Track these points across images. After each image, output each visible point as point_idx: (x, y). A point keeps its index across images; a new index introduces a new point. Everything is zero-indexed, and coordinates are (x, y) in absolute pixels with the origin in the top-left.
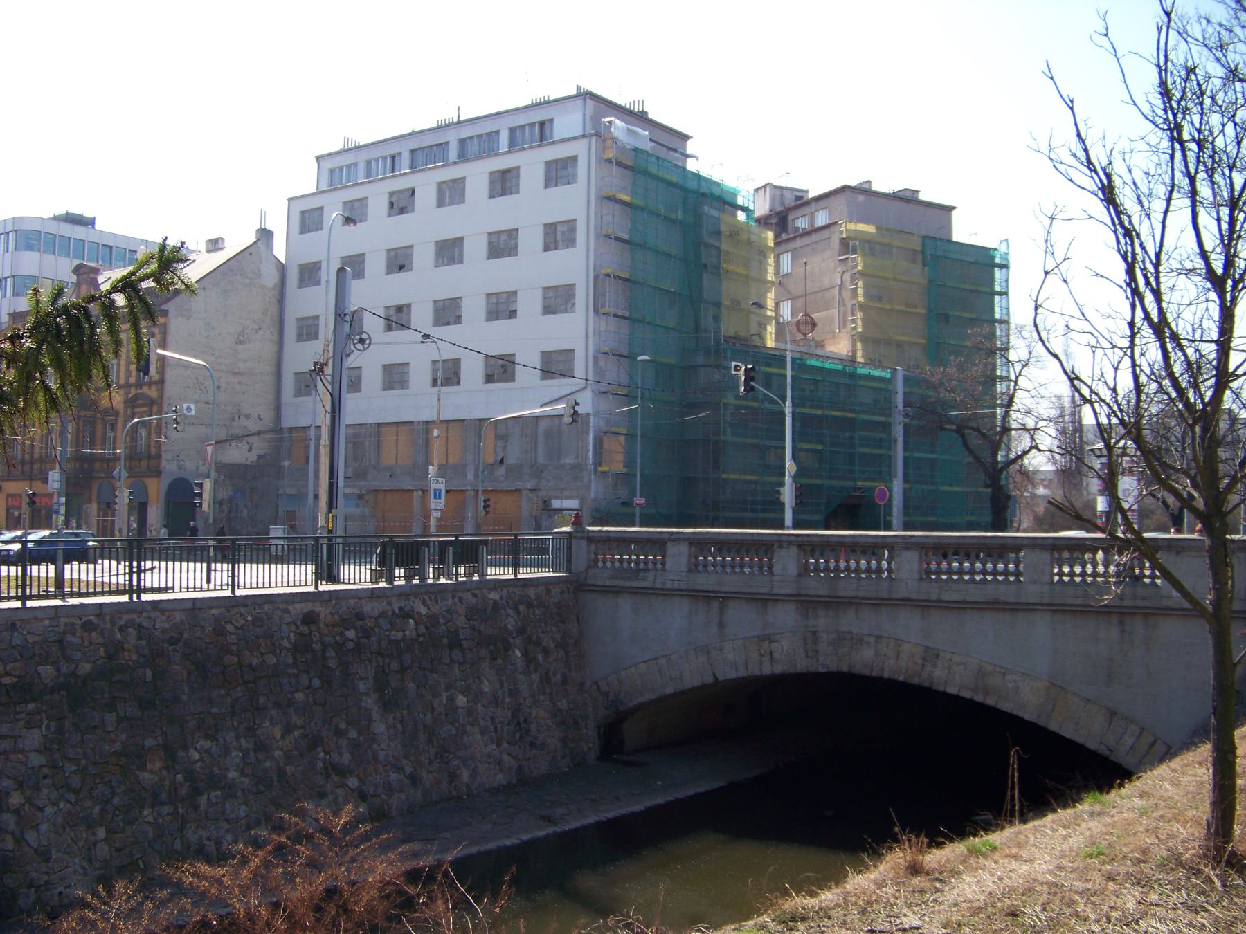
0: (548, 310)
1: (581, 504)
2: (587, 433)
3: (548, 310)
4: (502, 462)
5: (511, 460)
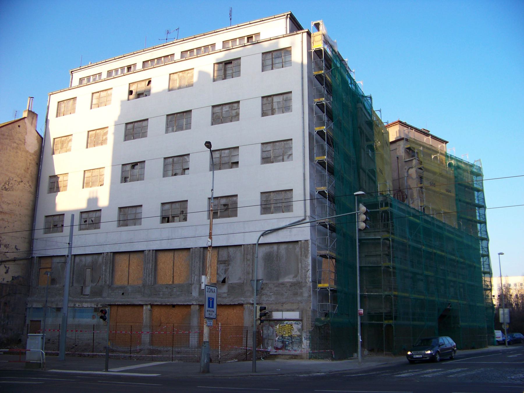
0: (266, 160)
1: (301, 315)
2: (306, 257)
3: (266, 160)
4: (224, 281)
5: (234, 279)
